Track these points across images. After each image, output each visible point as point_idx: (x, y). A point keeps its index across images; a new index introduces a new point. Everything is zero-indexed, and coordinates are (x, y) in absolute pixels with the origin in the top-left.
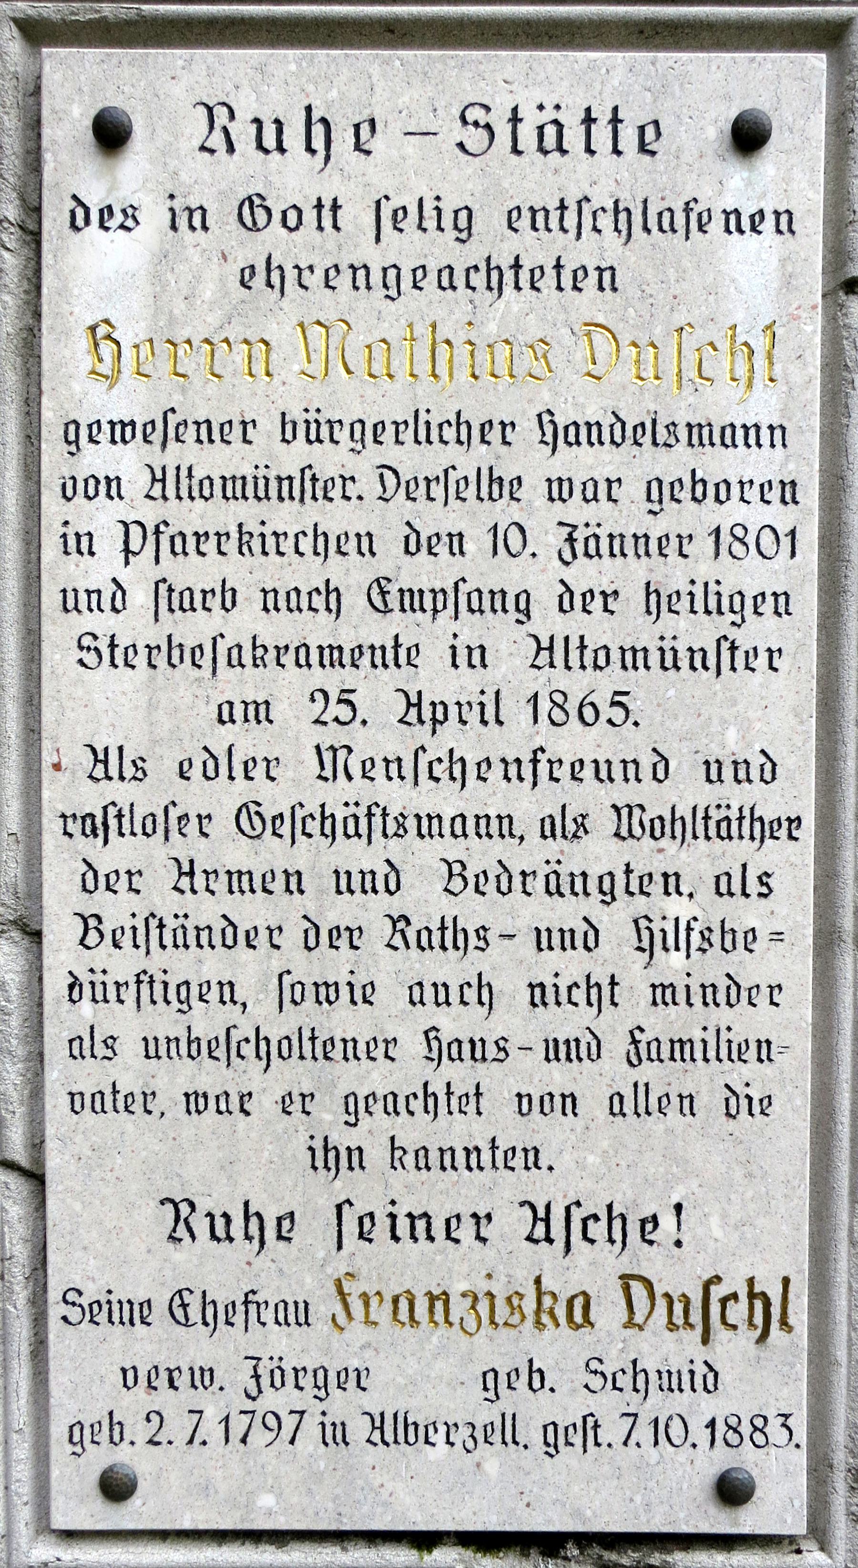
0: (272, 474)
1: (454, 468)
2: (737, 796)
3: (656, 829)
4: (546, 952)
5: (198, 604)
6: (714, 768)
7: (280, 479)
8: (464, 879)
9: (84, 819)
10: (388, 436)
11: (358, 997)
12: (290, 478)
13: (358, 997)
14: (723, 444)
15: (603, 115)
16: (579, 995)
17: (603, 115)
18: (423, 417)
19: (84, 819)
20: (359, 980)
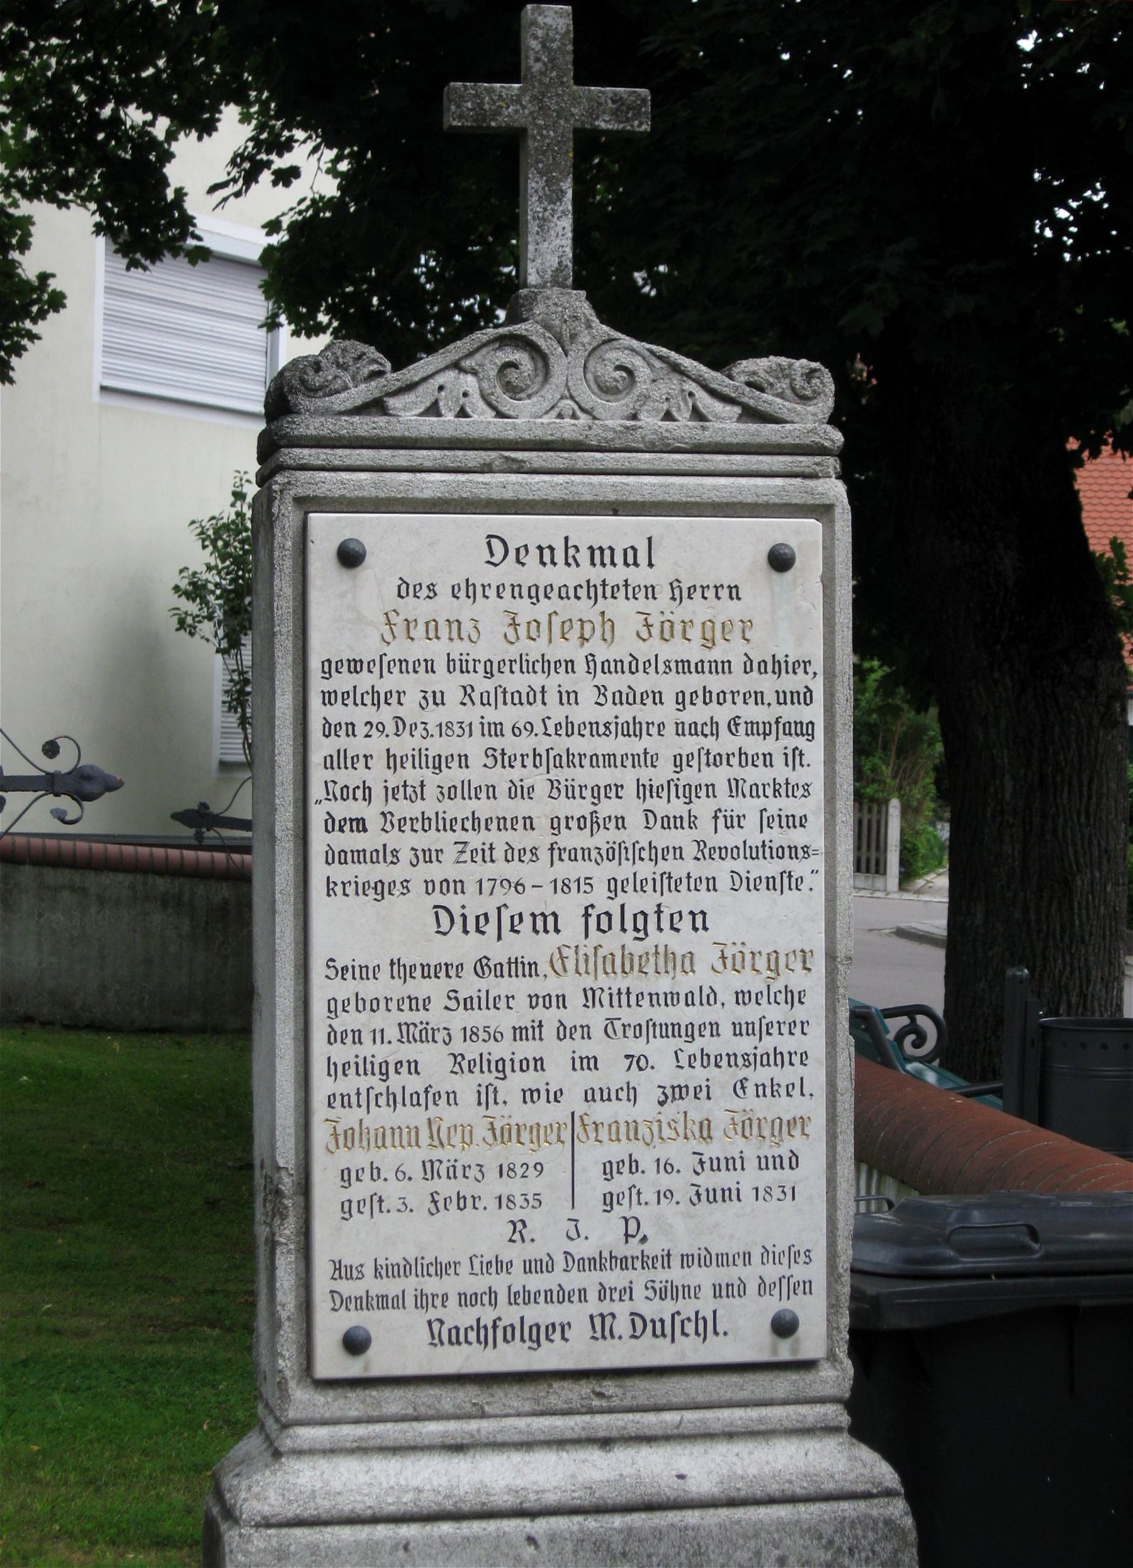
0: (734, 814)
1: (549, 718)
2: (615, 575)
3: (499, 971)
4: (524, 1041)
5: (577, 794)
6: (528, 826)
7: (581, 1059)
8: (559, 790)
9: (579, 819)
10: (774, 1030)
11: (552, 1098)
12: (361, 1298)
13: (552, 1098)
14: (751, 796)
15: (624, 991)
16: (582, 593)
17: (624, 991)
18: (524, 658)
19: (579, 819)
20: (553, 1088)
